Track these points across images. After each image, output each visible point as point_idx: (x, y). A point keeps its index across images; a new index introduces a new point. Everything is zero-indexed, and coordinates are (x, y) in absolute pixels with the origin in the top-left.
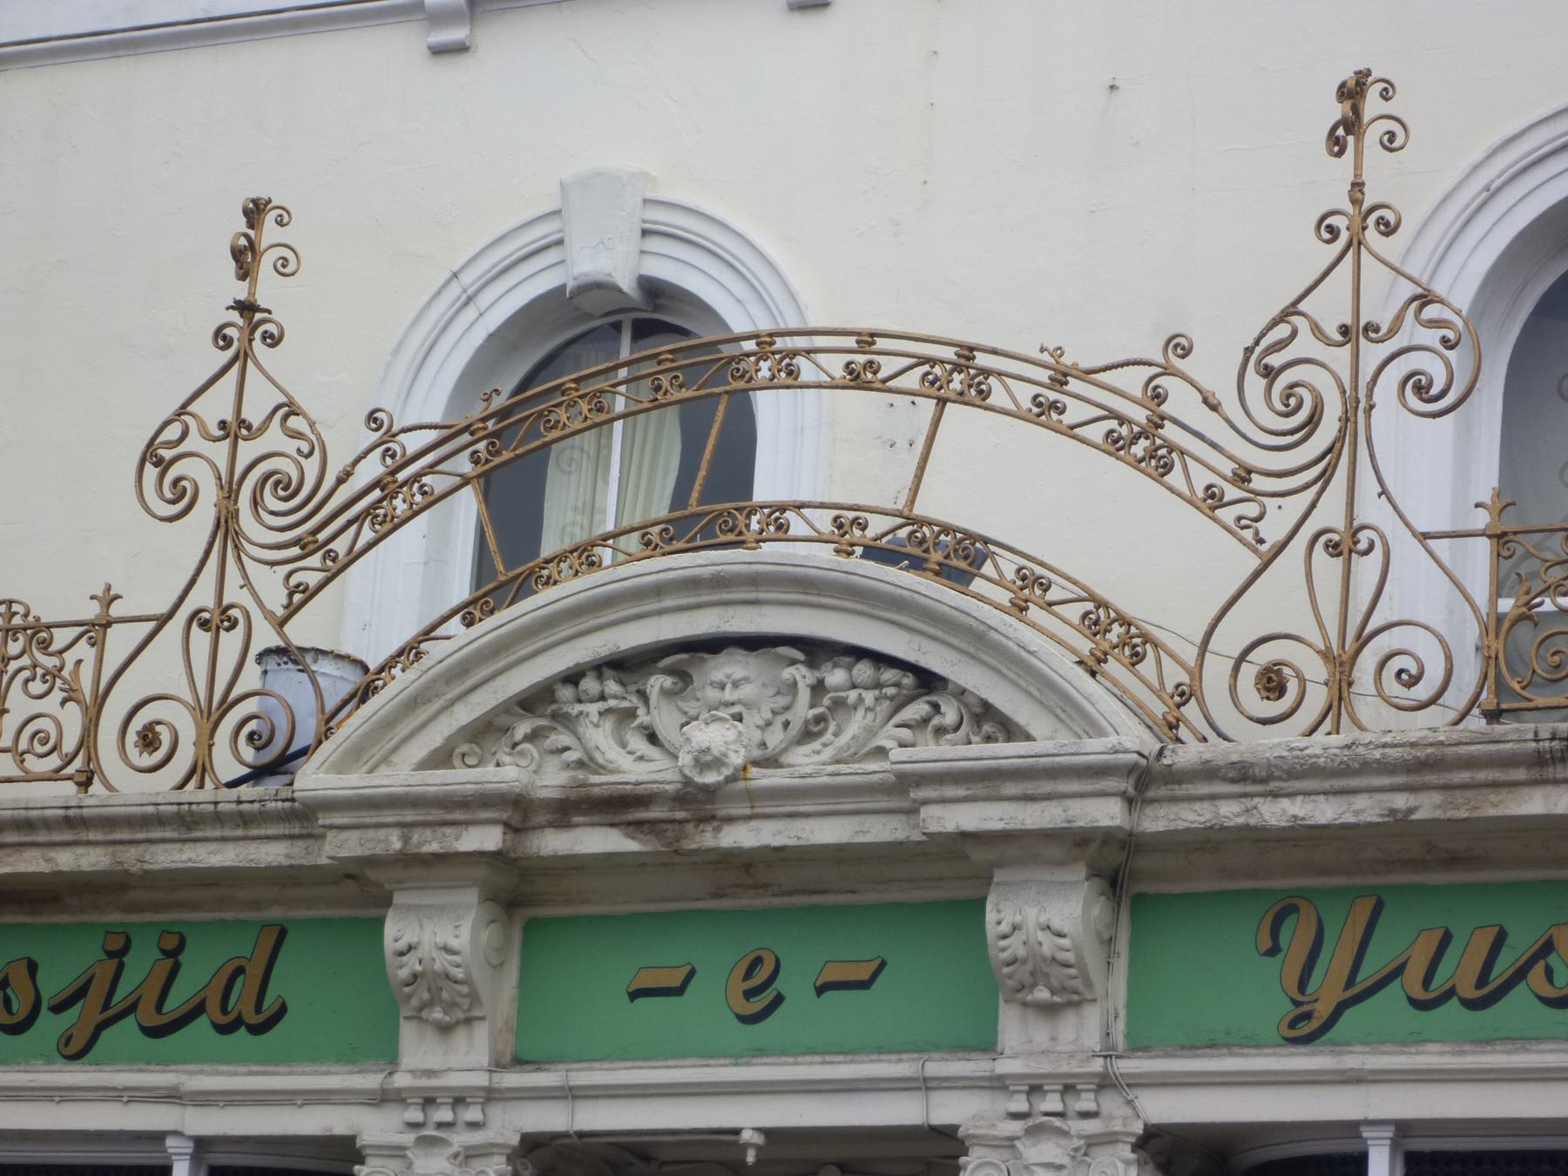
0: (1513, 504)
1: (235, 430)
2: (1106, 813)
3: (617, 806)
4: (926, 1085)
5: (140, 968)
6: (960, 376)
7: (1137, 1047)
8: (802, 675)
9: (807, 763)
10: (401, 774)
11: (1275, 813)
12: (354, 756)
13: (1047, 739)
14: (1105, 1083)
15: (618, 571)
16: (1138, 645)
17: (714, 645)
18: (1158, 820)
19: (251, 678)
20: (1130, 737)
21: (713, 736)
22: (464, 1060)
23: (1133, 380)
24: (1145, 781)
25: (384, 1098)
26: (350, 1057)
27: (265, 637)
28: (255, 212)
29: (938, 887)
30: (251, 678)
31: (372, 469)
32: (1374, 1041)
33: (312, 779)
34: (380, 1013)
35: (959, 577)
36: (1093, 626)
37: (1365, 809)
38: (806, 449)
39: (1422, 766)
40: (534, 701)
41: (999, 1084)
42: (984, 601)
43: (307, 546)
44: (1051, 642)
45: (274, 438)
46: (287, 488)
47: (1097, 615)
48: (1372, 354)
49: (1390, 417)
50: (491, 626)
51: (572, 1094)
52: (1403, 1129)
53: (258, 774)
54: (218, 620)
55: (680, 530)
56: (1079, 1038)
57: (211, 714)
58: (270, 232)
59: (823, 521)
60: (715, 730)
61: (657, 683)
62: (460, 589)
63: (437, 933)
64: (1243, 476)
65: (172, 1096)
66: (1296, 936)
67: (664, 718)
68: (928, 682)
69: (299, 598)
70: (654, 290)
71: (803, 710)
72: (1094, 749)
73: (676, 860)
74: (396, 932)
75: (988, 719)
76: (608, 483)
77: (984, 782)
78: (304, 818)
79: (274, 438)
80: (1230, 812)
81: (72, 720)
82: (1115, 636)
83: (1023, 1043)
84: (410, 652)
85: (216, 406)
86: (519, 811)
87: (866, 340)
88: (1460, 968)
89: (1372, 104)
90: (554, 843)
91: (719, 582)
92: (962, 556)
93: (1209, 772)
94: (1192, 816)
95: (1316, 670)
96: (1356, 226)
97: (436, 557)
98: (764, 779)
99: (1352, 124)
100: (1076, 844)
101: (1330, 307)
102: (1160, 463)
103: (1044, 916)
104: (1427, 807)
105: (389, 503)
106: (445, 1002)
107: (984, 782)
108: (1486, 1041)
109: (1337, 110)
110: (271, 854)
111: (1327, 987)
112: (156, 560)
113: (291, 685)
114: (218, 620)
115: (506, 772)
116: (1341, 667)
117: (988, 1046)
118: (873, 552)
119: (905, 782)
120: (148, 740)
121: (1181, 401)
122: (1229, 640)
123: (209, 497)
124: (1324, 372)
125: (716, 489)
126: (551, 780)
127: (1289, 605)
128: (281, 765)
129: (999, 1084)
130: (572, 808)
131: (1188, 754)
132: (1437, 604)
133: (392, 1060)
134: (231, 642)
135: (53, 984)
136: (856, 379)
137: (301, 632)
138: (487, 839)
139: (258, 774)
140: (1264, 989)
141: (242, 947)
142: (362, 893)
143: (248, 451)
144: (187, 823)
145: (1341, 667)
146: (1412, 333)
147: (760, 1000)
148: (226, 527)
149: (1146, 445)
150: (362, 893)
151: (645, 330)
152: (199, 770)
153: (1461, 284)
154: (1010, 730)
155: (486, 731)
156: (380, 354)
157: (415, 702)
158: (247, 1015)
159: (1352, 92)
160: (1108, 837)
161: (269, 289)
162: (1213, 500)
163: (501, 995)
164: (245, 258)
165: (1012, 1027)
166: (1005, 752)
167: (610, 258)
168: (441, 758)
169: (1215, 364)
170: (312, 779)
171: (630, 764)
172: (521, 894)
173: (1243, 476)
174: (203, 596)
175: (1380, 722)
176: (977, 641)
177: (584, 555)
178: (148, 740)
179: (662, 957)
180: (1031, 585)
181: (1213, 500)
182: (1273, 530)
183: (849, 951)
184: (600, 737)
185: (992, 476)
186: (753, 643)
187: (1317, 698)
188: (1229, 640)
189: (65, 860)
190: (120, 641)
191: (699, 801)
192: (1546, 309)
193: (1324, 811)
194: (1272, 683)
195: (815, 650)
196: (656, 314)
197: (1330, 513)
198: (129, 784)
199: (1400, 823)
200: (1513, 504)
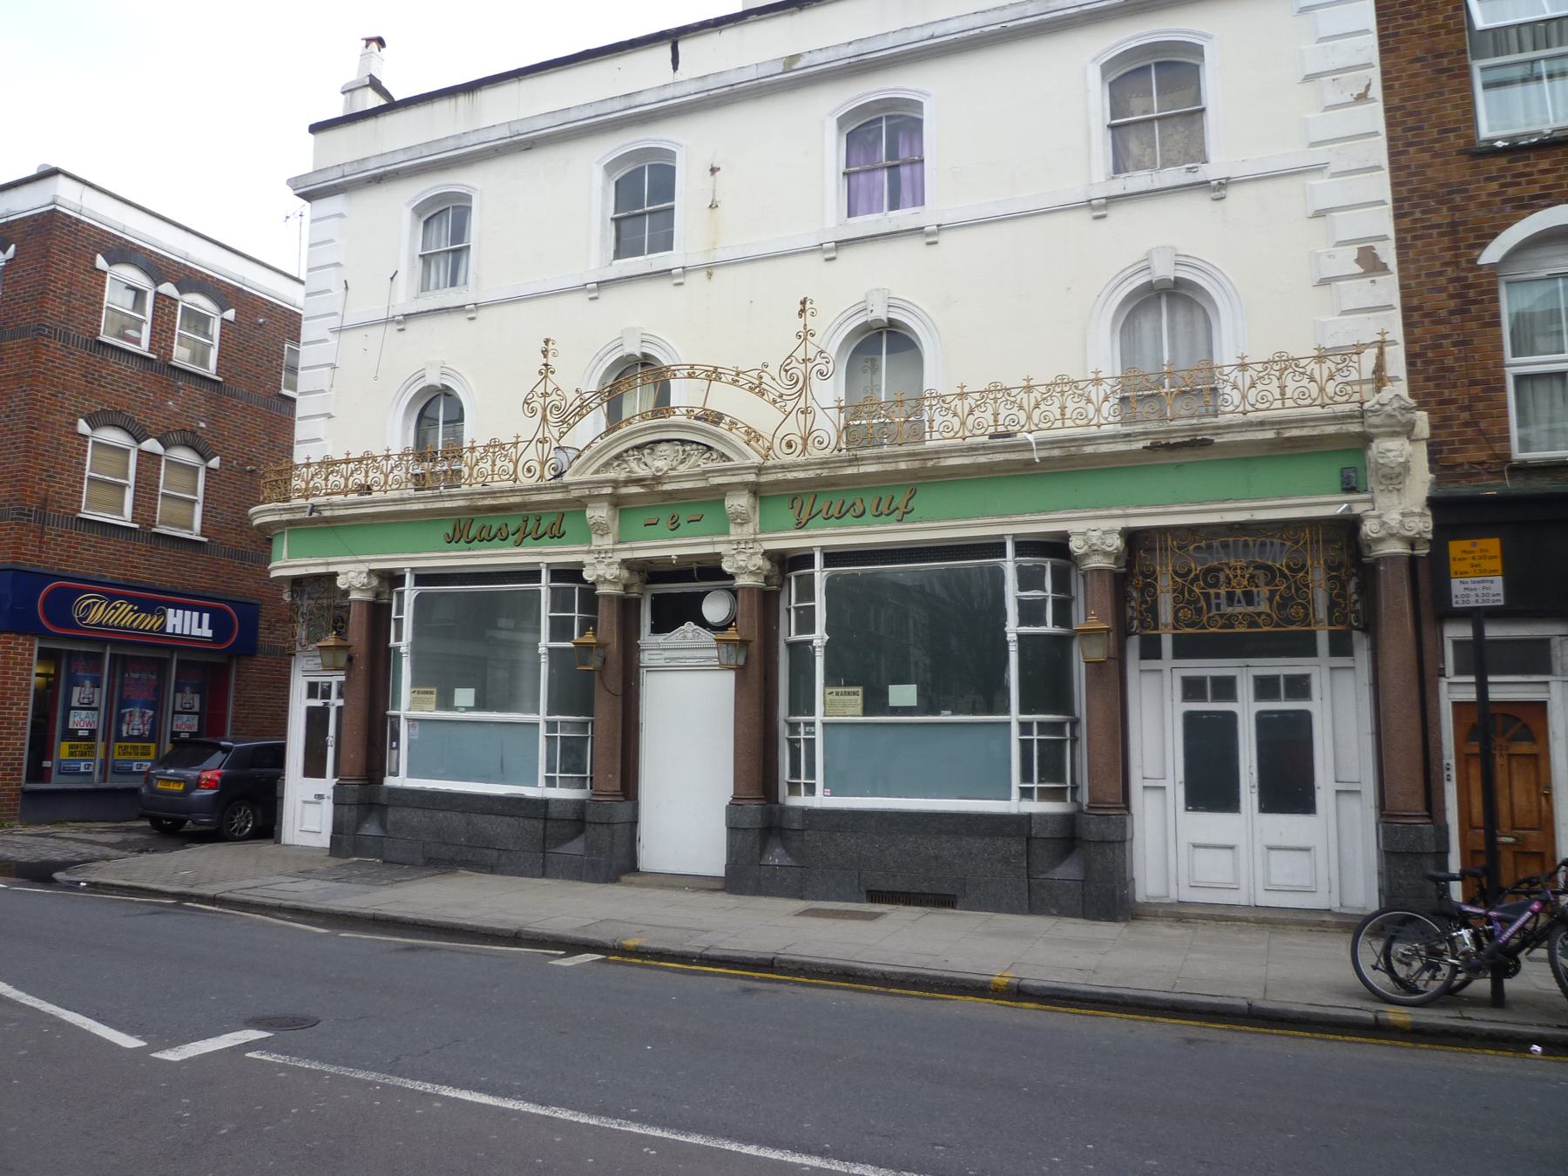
0: (330, 416)
1: (545, 395)
2: (752, 478)
3: (638, 481)
4: (714, 543)
5: (531, 524)
6: (714, 374)
7: (762, 532)
8: (680, 448)
9: (682, 469)
10: (587, 476)
11: (790, 476)
12: (576, 472)
13: (737, 461)
14: (754, 541)
15: (638, 424)
16: (758, 437)
17: (659, 442)
18: (763, 479)
19: (552, 454)
20: (756, 459)
21: (660, 464)
22: (606, 542)
23: (754, 374)
24: (760, 470)
25: (589, 552)
26: (581, 543)
27: (555, 445)
28: (547, 342)
29: (713, 497)
30: (552, 454)
31: (578, 402)
32: (815, 528)
33: (567, 478)
34: (587, 533)
35: (717, 423)
36: (747, 433)
37: (811, 474)
38: (683, 394)
39: (824, 463)
40: (618, 457)
41: (730, 542)
42: (722, 429)
43: (563, 422)
44: (737, 438)
45: (554, 396)
46: (558, 408)
47: (749, 431)
48: (810, 365)
49: (815, 381)
50: (607, 439)
51: (632, 549)
52: (823, 548)
53: (555, 477)
54: (543, 441)
55: (655, 414)
56: (748, 530)
57: (543, 464)
58: (550, 346)
59: (684, 410)
60: (659, 462)
61: (646, 451)
62: (1377, 441)
63: (599, 513)
64: (781, 396)
65: (540, 554)
66: (797, 505)
67: (648, 459)
68: (709, 448)
69: (562, 434)
70: (645, 355)
71: (681, 457)
72: (748, 463)
73: (653, 494)
74: (589, 513)
75: (723, 456)
76: (637, 402)
77: (723, 472)
78: (566, 487)
79: (554, 396)
80: (780, 476)
81: (511, 466)
82: (753, 435)
83: (736, 532)
84: (588, 446)
85: (540, 389)
86: (615, 483)
87: (692, 366)
88: (834, 510)
89: (808, 305)
90: (624, 491)
91: (659, 427)
92: (717, 418)
93: (775, 467)
94: (771, 478)
95: (799, 441)
96: (805, 335)
97: (596, 423)
98: (673, 473)
99: (803, 311)
100: (745, 485)
101: (800, 355)
102: (762, 394)
103: (739, 502)
104: (825, 473)
105: (582, 410)
106: (602, 529)
107: (723, 472)
108: (841, 526)
109: (799, 307)
110: (559, 496)
111: (804, 515)
112: (529, 427)
113: (562, 455)
114: (543, 441)
115: (611, 474)
116: (805, 440)
117: (728, 533)
118: (697, 418)
119: (705, 472)
120: (529, 470)
121: (766, 379)
122: (780, 435)
123: (540, 411)
124: (799, 370)
125: (662, 403)
126: (623, 476)
127: (793, 427)
128: (560, 475)
129: (730, 542)
130: (627, 482)
131: (770, 463)
132: (827, 425)
133: (591, 544)
134: (547, 446)
135: (512, 529)
136: (690, 376)
137: (563, 443)
138: (608, 490)
139: (555, 477)
140: (790, 517)
141: (554, 519)
142: (580, 504)
143: (548, 400)
144: (539, 490)
145: (805, 440)
146: (819, 360)
147: (675, 525)
148: (544, 419)
149: (758, 389)
150: (580, 504)
151: (644, 365)
152: (541, 477)
153: (832, 350)
154: (729, 459)
155: (607, 465)
156: (581, 374)
157: (589, 459)
158: (557, 535)
159: (803, 303)
160: (753, 483)
161: (551, 360)
162: (775, 402)
163: (615, 527)
164: (545, 353)
165: (733, 529)
166: (728, 464)
167: (880, 313)
168: (597, 472)
169: (774, 370)
170: (567, 478)
171: (641, 471)
172: (618, 503)
173: (781, 396)
174: (540, 436)
175: (815, 454)
176: (720, 438)
177: (629, 422)
178: (529, 470)
179: (652, 516)
180: (733, 423)
181: (775, 402)
182: (788, 409)
183: (694, 512)
184: (634, 465)
185: (723, 398)
186: (668, 441)
187: (800, 448)
188: (780, 435)
189: (512, 500)
190: (521, 446)
191: (657, 479)
192: (854, 351)
193: (802, 475)
194: (789, 445)
195: (683, 442)
196: (646, 361)
197: (801, 404)
198: (526, 481)
199: (819, 477)
200: (330, 416)
